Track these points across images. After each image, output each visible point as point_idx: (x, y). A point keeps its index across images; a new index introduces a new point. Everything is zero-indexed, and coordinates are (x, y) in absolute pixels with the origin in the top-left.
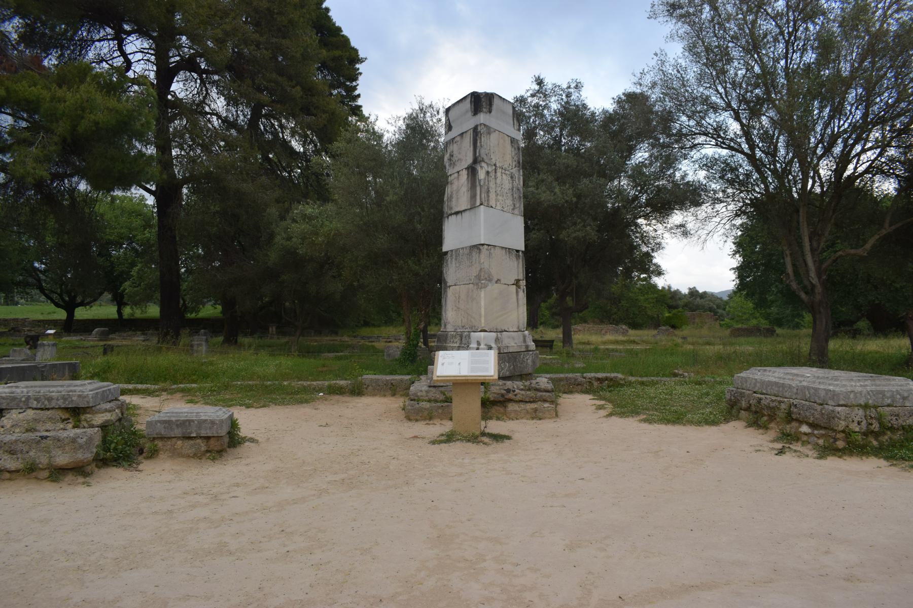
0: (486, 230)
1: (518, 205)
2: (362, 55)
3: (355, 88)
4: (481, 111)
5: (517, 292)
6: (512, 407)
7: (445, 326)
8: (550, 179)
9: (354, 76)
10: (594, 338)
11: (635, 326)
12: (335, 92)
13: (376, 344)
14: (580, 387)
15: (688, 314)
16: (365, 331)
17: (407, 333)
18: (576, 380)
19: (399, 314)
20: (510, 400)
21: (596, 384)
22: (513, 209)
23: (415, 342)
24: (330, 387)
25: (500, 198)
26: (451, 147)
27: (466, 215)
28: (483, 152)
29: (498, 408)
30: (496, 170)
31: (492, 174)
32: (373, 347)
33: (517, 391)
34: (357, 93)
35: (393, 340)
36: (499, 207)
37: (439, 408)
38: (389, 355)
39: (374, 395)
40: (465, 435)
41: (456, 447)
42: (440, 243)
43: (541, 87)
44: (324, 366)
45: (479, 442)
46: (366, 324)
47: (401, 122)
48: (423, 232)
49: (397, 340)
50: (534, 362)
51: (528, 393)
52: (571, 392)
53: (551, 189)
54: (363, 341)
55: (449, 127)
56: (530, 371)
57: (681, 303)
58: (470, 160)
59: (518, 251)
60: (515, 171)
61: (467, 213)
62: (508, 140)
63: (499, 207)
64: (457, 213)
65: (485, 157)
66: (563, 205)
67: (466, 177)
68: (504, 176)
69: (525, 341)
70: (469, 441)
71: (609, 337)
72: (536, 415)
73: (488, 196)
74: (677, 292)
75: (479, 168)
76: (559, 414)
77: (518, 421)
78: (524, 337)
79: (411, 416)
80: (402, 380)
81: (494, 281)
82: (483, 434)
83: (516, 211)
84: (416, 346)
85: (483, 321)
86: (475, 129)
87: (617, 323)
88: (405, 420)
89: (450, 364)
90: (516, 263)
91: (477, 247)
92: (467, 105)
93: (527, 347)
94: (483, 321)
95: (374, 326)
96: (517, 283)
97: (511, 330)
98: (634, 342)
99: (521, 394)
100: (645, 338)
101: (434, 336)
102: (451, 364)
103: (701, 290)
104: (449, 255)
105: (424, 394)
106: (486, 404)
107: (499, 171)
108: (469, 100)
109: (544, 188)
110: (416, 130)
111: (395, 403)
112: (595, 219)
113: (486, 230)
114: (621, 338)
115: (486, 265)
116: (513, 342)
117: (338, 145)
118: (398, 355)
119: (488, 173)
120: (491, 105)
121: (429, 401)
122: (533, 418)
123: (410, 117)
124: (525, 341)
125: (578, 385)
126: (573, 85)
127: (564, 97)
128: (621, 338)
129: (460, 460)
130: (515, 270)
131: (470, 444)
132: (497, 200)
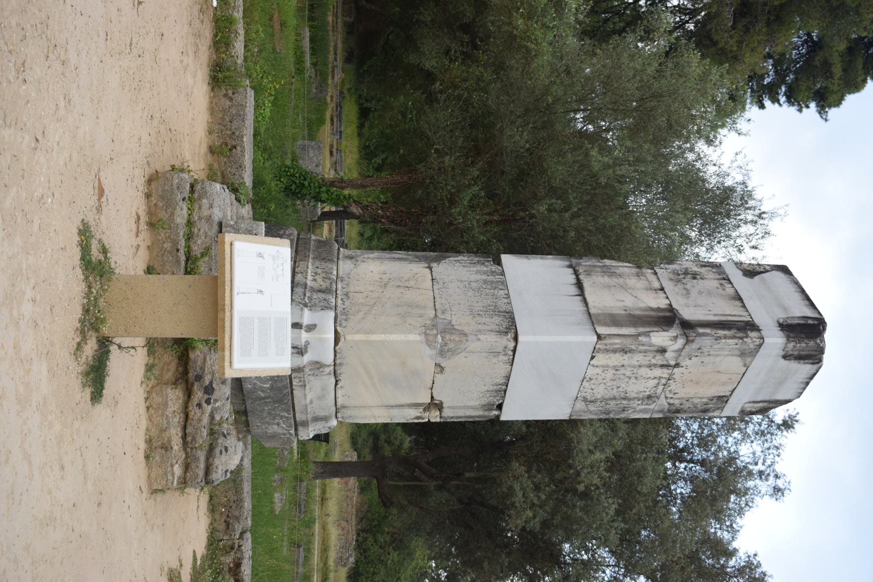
0: (542, 342)
1: (592, 408)
2: (832, 112)
3: (775, 100)
4: (788, 338)
5: (416, 405)
6: (174, 397)
7: (351, 258)
8: (619, 444)
9: (795, 98)
10: (332, 507)
12: (769, 65)
13: (327, 128)
14: (222, 527)
16: (351, 110)
17: (342, 181)
18: (237, 519)
19: (379, 169)
20: (189, 393)
21: (228, 560)
22: (585, 400)
23: (324, 196)
24: (231, 21)
25: (610, 374)
26: (711, 275)
27: (576, 304)
28: (705, 340)
29: (173, 366)
30: (667, 366)
31: (659, 359)
32: (322, 122)
33: (208, 409)
34: (767, 103)
35: (332, 155)
36: (591, 371)
37: (175, 243)
38: (304, 148)
39: (212, 111)
40: (101, 302)
41: (70, 284)
42: (511, 251)
43: (779, 427)
44: (283, 24)
45: (83, 333)
46: (364, 113)
47: (739, 178)
48: (532, 216)
49: (335, 165)
50: (274, 436)
51: (205, 432)
52: (212, 508)
53: (598, 446)
54: (333, 105)
55: (751, 272)
56: (255, 430)
58: (688, 313)
59: (500, 407)
60: (663, 403)
61: (581, 307)
62: (724, 391)
63: (591, 371)
64: (579, 285)
65: (694, 346)
66: (570, 467)
67: (654, 305)
68: (653, 382)
69: (316, 419)
70: (86, 311)
71: (334, 533)
72: (155, 448)
73: (615, 351)
75: (674, 331)
76: (159, 497)
77: (142, 408)
78: (326, 419)
79: (163, 189)
80: (241, 167)
81: (439, 360)
82: (104, 344)
83: (580, 405)
84: (317, 198)
85: (358, 337)
86: (750, 326)
87: (361, 547)
88: (149, 171)
89: (259, 270)
90: (476, 403)
91: (511, 328)
92: (799, 310)
93: (305, 424)
94: (358, 337)
95: (361, 126)
96: (435, 405)
99: (202, 418)
101: (341, 230)
104: (494, 268)
105: (206, 213)
106: (183, 347)
107: (665, 373)
108: (809, 313)
109: (601, 431)
110: (721, 207)
111: (193, 152)
112: (545, 524)
113: (542, 342)
115: (473, 345)
116: (314, 397)
117: (694, 61)
118: (307, 165)
119: (663, 351)
120: (800, 358)
121: (190, 223)
122: (149, 441)
123: (747, 195)
124: (316, 419)
126: (780, 483)
127: (760, 467)
128: (332, 555)
129: (29, 294)
130: (462, 402)
131: (78, 313)
132: (605, 368)
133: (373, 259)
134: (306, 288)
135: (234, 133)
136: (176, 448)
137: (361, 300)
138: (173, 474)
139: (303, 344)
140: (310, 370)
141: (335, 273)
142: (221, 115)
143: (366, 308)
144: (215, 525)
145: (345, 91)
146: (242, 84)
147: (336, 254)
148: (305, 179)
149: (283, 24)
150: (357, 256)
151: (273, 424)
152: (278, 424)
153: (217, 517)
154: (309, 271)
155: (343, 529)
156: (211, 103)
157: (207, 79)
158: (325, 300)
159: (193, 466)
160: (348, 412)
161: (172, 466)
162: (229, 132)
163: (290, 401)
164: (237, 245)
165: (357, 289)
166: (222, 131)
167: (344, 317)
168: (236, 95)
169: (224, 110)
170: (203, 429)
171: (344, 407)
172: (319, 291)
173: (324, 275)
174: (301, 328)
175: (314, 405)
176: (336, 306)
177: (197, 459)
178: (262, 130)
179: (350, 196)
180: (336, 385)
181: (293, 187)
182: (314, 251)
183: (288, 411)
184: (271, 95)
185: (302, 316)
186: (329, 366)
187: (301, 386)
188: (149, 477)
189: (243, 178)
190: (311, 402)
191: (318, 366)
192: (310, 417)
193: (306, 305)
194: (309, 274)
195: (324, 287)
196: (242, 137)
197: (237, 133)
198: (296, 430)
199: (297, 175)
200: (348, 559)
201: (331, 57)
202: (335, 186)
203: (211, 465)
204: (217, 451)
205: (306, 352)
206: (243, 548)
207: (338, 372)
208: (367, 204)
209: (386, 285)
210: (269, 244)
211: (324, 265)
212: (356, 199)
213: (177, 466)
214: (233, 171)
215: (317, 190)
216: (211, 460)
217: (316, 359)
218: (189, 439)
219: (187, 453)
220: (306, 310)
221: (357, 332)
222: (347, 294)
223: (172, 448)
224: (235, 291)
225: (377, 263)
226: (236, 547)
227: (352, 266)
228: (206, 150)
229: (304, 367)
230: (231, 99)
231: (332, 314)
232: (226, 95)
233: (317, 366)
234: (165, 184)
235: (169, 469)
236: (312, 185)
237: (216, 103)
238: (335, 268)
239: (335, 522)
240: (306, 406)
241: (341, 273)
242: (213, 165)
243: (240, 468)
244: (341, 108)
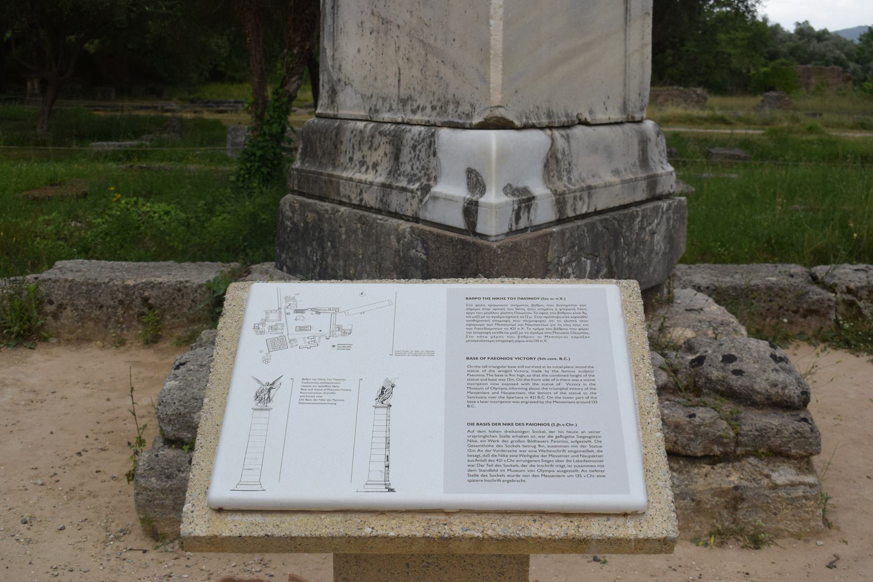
7: (333, 93)
11: (717, 89)
14: (814, 322)
15: (798, 68)
16: (214, 91)
23: (275, 129)
39: (83, 340)
50: (670, 239)
51: (703, 414)
57: (784, 49)
69: (644, 161)
74: (777, 28)
80: (180, 289)
85: (496, 77)
88: (137, 539)
93: (653, 181)
95: (232, 80)
97: (601, 117)
98: (722, 121)
100: (741, 113)
102: (319, 391)
103: (817, 27)
114: (696, 112)
122: (722, 537)
124: (644, 161)
125: (810, 312)
128: (696, 112)
133: (335, 50)
134: (390, 186)
135: (121, 302)
136: (734, 478)
137: (416, 72)
138: (793, 485)
139: (509, 199)
140: (560, 179)
141: (360, 125)
142: (91, 324)
143: (433, 61)
144: (810, 333)
145: (192, 97)
146: (32, 286)
147: (329, 122)
148: (254, 154)
149: (52, 183)
150: (330, 81)
151: (652, 242)
152: (653, 233)
153: (796, 330)
154: (357, 176)
155: (667, 100)
156: (69, 341)
157: (23, 351)
158: (414, 147)
159: (776, 442)
160: (634, 100)
161: (775, 487)
162: (120, 311)
163: (616, 214)
164: (222, 489)
165: (393, 80)
166: (118, 322)
167: (451, 107)
168: (53, 298)
169: (82, 319)
170: (697, 420)
171: (624, 108)
172: (397, 158)
173: (365, 148)
174: (476, 203)
175: (622, 167)
176: (428, 125)
177: (762, 433)
178: (183, 215)
179: (275, 93)
180: (586, 123)
181: (264, 170)
182: (321, 165)
183: (632, 217)
184: (136, 203)
185: (449, 200)
186: (553, 140)
187: (590, 196)
188: (798, 536)
189: (200, 286)
190: (616, 172)
191: (552, 161)
192: (641, 174)
193: (426, 189)
194: (363, 177)
195: (388, 149)
196: (127, 287)
197: (121, 296)
198: (660, 198)
199: (249, 165)
200: (698, 95)
201: (142, 113)
202: (263, 114)
203: (769, 398)
204: (737, 382)
205: (525, 190)
206: (852, 286)
207: (564, 119)
208: (284, 69)
209: (385, 22)
210: (234, 354)
211: (346, 146)
212: (278, 85)
213: (774, 476)
214: (188, 302)
215: (267, 137)
216: (758, 398)
217: (539, 168)
218: (717, 450)
219: (747, 455)
220: (439, 189)
221: (485, 79)
222: (404, 102)
223: (736, 488)
224: (379, 497)
225: (342, 40)
226: (850, 297)
227: (349, 90)
228: (151, 351)
229: (555, 192)
230: (61, 307)
231: (445, 134)
232: (55, 316)
233: (552, 165)
234: (162, 506)
235: (782, 493)
236: (261, 145)
237: (70, 333)
238: (352, 124)
239: (660, 110)
240: (623, 182)
241: (362, 113)
242: (179, 339)
243: (719, 295)
244: (209, 102)
